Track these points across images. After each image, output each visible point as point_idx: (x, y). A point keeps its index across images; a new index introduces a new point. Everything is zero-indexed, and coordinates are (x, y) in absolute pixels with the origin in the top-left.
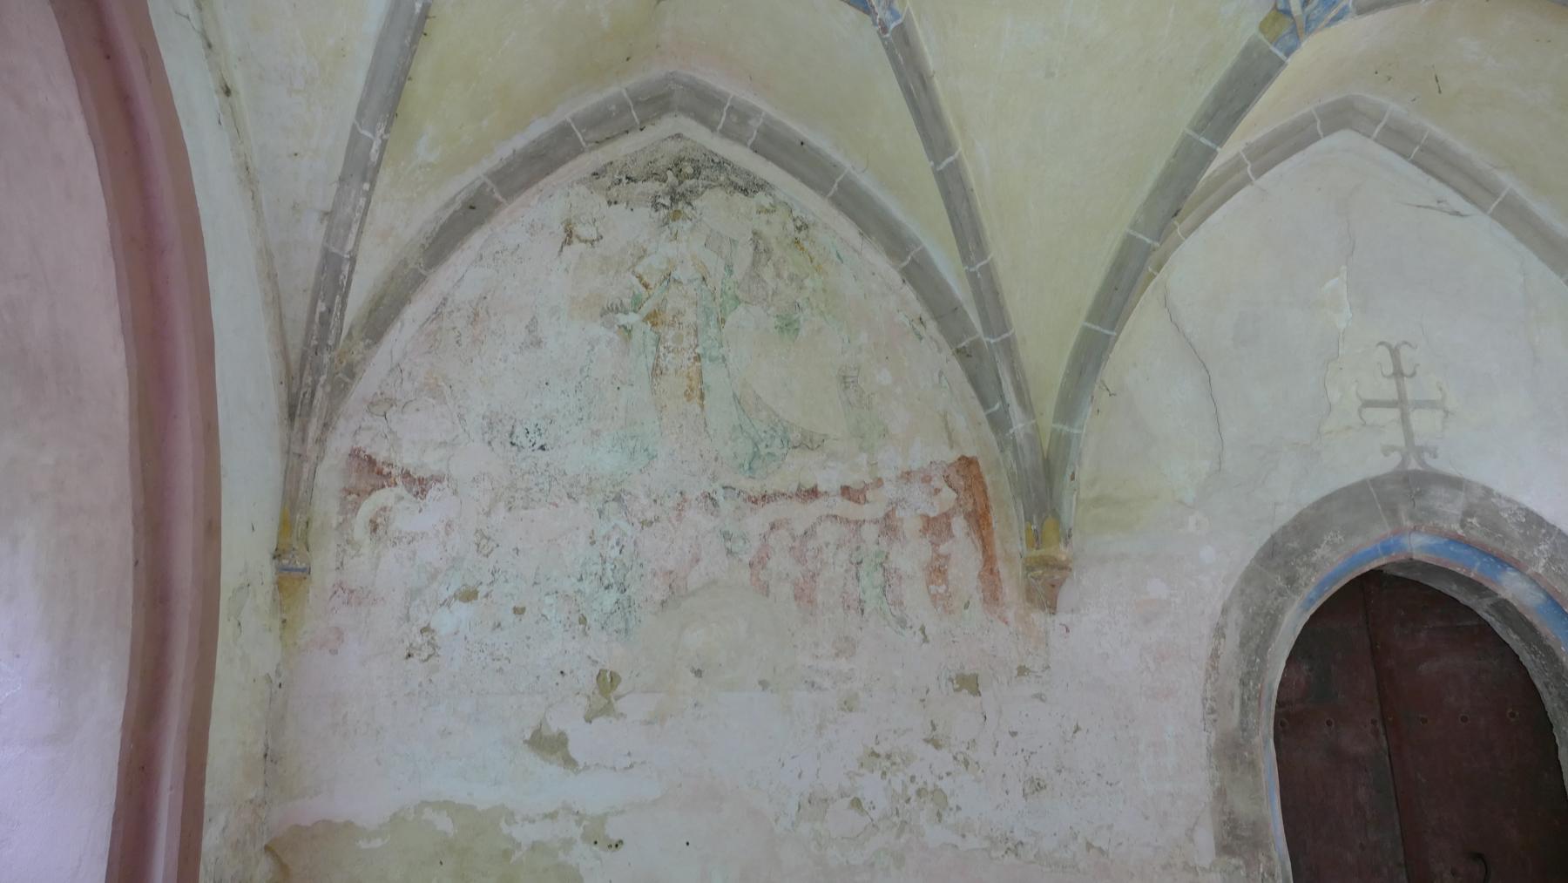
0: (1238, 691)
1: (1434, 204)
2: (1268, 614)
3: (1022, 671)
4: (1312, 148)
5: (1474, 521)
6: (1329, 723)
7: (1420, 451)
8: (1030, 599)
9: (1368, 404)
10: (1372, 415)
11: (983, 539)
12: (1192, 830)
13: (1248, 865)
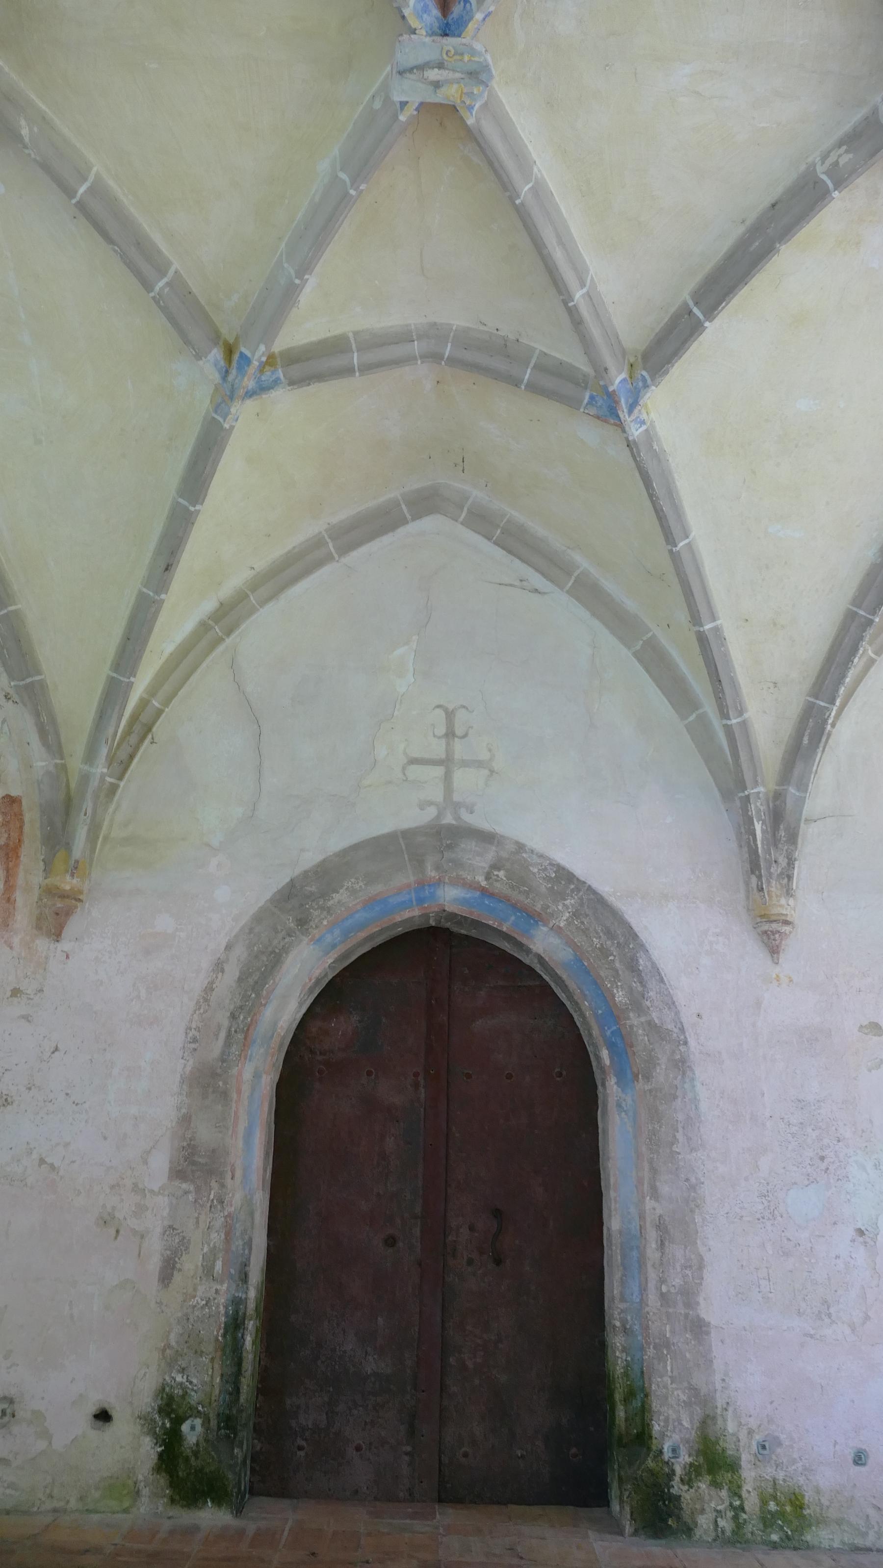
0: (226, 1023)
1: (517, 583)
2: (273, 952)
3: (16, 992)
4: (402, 531)
5: (501, 874)
6: (369, 1073)
7: (457, 806)
8: (38, 927)
9: (414, 761)
10: (415, 771)
11: (8, 870)
12: (148, 1152)
13: (198, 1190)
